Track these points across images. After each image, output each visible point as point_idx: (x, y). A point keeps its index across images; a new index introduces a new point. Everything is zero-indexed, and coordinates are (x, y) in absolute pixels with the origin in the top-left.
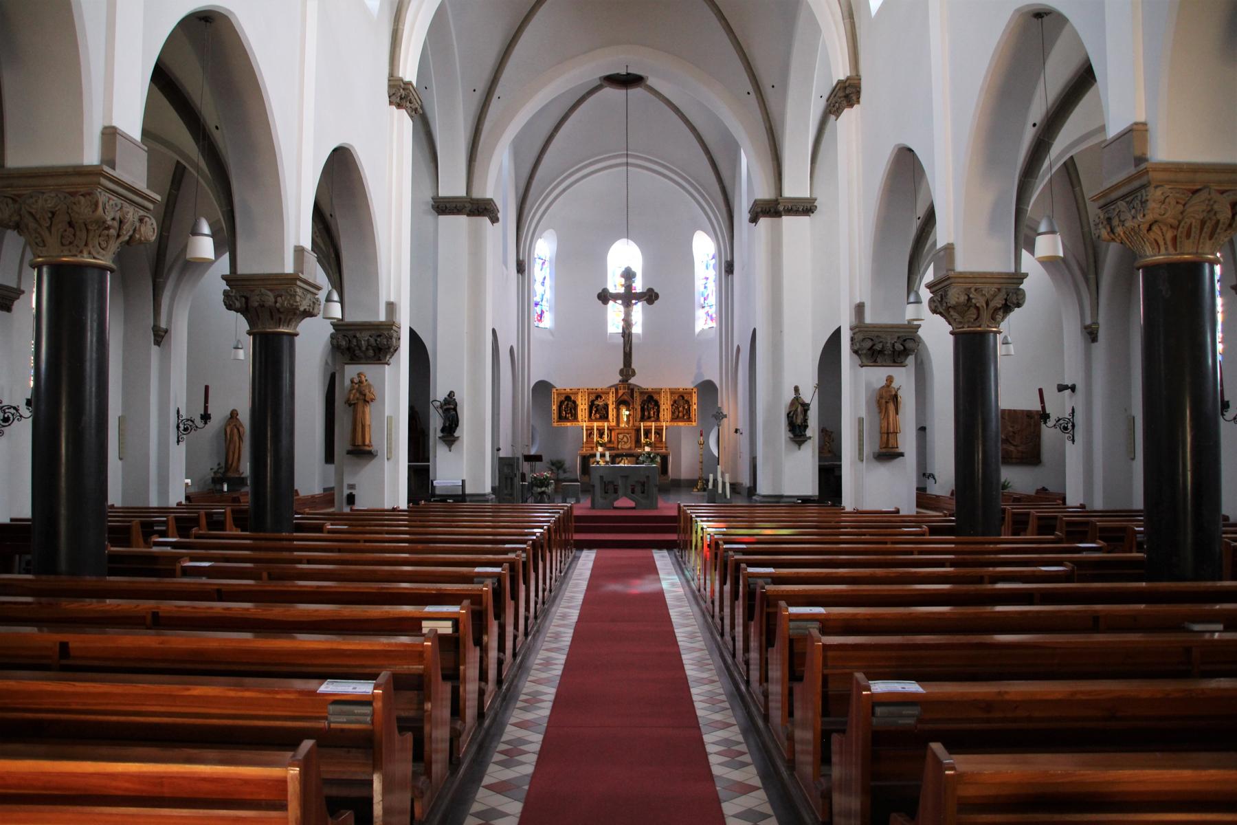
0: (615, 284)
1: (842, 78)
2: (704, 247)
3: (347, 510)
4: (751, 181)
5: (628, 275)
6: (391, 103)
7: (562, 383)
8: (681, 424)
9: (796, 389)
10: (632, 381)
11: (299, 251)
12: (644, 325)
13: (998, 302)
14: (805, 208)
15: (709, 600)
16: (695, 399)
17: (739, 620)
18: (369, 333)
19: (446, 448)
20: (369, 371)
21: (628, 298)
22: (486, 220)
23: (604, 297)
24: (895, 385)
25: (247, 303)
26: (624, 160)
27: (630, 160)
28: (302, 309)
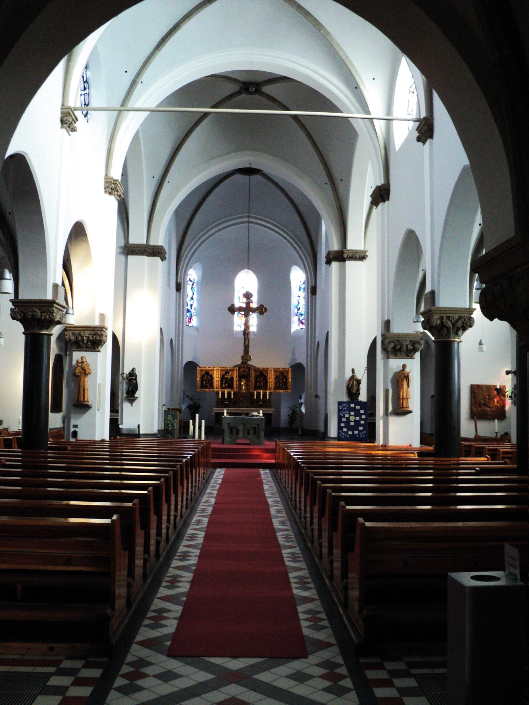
0: (239, 302)
1: (379, 184)
2: (298, 277)
3: (74, 440)
4: (328, 238)
5: (248, 296)
6: (105, 192)
7: (203, 364)
8: (281, 391)
9: (353, 371)
10: (250, 363)
11: (56, 286)
12: (258, 326)
13: (460, 324)
14: (360, 256)
15: (290, 492)
16: (290, 375)
17: (316, 515)
18: (88, 332)
19: (129, 405)
20: (88, 356)
21: (247, 310)
22: (158, 259)
23: (232, 310)
24: (407, 370)
25: (24, 316)
26: (247, 219)
27: (251, 220)
28: (56, 320)
